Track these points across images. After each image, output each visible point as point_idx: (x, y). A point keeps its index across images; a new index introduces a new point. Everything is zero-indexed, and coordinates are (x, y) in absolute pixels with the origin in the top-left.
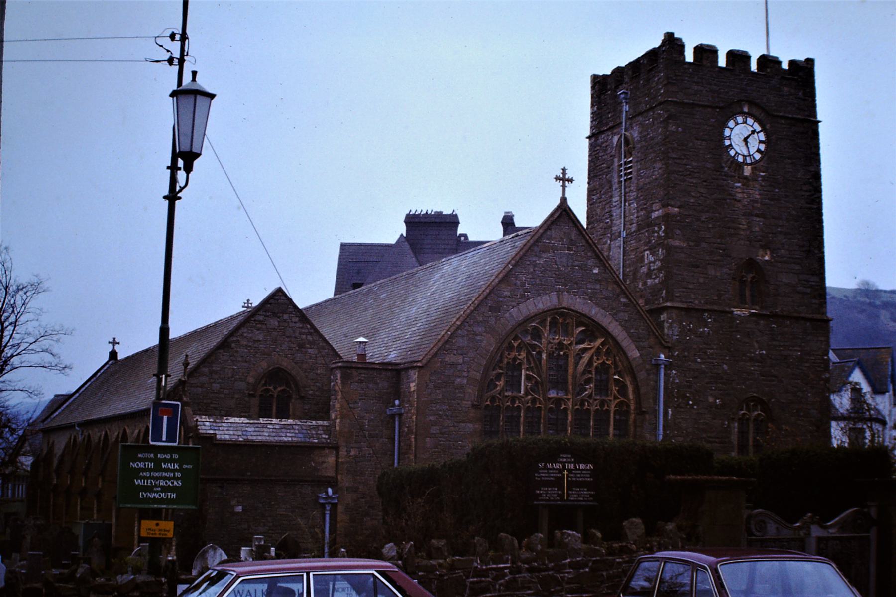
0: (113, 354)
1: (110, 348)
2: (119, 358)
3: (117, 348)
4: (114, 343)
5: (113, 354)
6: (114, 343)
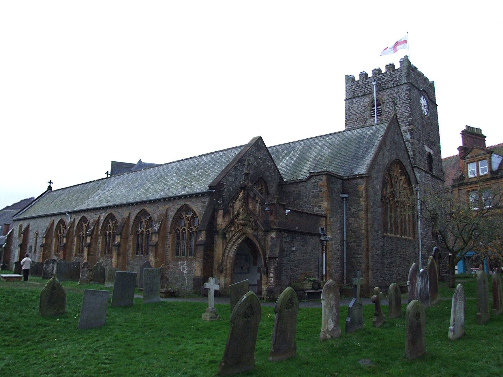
0: (50, 188)
1: (49, 184)
2: (53, 190)
3: (52, 185)
4: (50, 182)
5: (50, 188)
6: (50, 182)
